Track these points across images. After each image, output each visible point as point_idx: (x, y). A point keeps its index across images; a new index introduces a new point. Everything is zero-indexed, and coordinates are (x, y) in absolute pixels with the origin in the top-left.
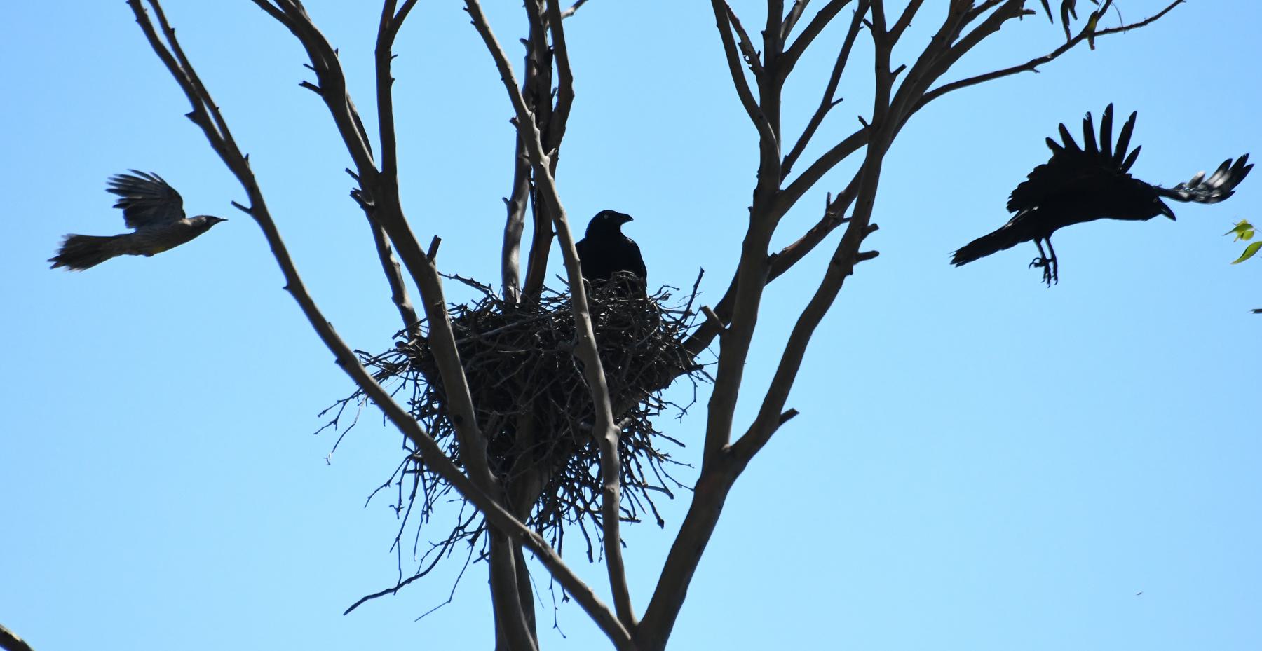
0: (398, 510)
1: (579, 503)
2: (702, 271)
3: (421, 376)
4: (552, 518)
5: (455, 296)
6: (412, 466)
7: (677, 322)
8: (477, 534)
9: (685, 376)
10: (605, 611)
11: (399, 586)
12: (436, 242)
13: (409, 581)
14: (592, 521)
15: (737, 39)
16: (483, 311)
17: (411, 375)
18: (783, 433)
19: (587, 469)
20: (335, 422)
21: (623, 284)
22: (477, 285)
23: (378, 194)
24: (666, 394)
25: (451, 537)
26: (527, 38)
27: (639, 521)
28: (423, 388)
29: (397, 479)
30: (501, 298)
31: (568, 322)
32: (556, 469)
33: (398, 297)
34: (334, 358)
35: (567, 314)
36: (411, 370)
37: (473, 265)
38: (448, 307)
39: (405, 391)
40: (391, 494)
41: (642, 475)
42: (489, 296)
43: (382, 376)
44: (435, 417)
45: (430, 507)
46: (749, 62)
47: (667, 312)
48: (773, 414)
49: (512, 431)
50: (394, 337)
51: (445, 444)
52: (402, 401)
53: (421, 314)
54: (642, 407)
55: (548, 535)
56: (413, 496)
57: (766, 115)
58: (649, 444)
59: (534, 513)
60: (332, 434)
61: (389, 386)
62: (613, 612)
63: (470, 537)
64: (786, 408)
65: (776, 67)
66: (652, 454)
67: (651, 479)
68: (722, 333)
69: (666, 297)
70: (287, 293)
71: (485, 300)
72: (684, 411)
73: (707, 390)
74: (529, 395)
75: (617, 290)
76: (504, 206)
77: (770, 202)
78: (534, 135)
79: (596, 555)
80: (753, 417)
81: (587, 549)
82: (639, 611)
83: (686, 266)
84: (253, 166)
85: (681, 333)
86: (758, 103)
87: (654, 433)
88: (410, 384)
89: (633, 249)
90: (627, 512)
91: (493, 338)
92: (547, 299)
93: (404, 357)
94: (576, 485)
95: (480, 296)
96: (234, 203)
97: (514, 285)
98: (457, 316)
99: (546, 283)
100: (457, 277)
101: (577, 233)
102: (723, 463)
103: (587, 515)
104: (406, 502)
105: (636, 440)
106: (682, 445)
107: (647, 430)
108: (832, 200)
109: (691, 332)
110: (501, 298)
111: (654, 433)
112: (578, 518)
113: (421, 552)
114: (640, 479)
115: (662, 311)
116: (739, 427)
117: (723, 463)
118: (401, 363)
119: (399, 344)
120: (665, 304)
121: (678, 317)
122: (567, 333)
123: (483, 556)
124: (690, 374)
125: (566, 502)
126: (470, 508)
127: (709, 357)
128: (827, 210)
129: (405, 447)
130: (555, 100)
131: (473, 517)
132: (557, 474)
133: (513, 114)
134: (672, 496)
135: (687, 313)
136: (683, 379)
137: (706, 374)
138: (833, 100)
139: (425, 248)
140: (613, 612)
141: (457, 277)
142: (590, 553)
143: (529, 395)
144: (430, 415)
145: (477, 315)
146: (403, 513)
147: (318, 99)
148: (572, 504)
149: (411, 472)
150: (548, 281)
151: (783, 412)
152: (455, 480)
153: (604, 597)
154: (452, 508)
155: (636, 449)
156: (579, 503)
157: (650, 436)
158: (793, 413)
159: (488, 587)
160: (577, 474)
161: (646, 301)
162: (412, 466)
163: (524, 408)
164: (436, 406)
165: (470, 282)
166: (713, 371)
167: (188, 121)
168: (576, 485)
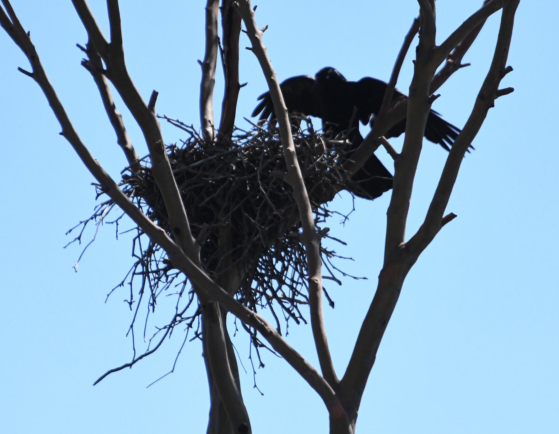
0: (131, 304)
1: (269, 292)
3: (142, 201)
5: (172, 137)
6: (140, 268)
10: (314, 372)
11: (134, 362)
13: (141, 358)
14: (280, 306)
16: (190, 145)
20: (79, 238)
23: (105, 58)
24: (331, 206)
26: (202, 61)
29: (128, 280)
33: (122, 141)
37: (182, 116)
45: (154, 301)
49: (214, 238)
56: (142, 292)
60: (77, 248)
62: (320, 373)
63: (189, 321)
64: (446, 213)
70: (62, 137)
71: (190, 139)
80: (421, 221)
82: (340, 372)
84: (33, 39)
91: (198, 167)
92: (238, 136)
94: (266, 278)
96: (20, 69)
102: (400, 257)
103: (274, 301)
104: (136, 297)
113: (149, 335)
116: (411, 229)
117: (400, 257)
123: (197, 335)
125: (259, 292)
129: (133, 255)
134: (340, 283)
139: (146, 101)
140: (320, 373)
143: (227, 210)
145: (184, 152)
146: (134, 306)
148: (263, 293)
151: (444, 215)
153: (313, 361)
156: (269, 292)
158: (452, 216)
159: (201, 361)
162: (140, 268)
163: (225, 221)
168: (266, 278)
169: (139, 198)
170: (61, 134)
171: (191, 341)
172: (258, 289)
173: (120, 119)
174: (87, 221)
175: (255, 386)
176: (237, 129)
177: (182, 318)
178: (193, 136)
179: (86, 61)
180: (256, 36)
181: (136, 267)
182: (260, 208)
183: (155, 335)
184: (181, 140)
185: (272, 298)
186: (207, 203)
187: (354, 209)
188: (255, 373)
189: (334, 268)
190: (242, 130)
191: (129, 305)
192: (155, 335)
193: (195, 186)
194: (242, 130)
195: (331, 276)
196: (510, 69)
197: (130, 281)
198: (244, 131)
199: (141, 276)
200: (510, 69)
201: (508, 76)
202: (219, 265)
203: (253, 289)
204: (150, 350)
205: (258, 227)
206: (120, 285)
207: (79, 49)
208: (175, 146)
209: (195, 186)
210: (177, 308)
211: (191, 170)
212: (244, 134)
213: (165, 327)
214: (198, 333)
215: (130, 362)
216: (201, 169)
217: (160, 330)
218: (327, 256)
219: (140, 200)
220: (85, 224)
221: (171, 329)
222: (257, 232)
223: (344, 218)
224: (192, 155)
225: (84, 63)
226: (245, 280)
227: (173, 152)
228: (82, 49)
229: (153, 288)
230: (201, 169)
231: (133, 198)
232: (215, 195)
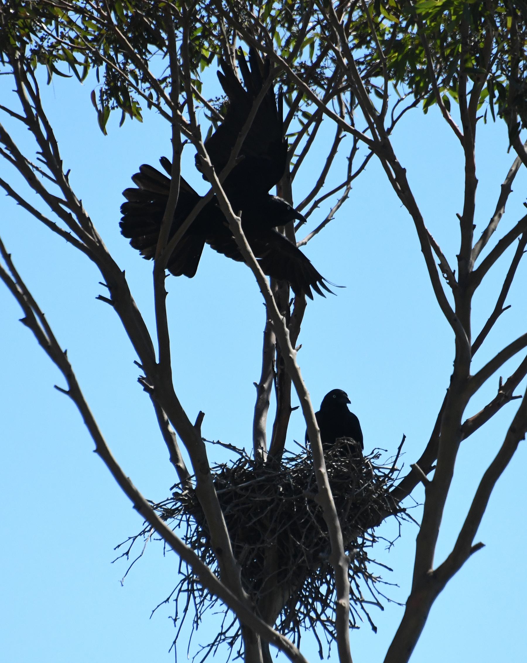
0: (175, 620)
1: (312, 614)
2: (404, 437)
3: (192, 518)
5: (218, 457)
7: (386, 476)
8: (234, 638)
9: (392, 517)
12: (201, 416)
14: (322, 628)
15: (437, 261)
16: (239, 467)
17: (184, 518)
18: (473, 562)
19: (317, 588)
20: (127, 553)
21: (344, 446)
22: (234, 449)
24: (378, 531)
25: (215, 641)
27: (358, 628)
28: (194, 527)
29: (174, 596)
30: (252, 458)
31: (307, 474)
32: (295, 588)
33: (174, 458)
34: (132, 504)
35: (301, 471)
36: (184, 513)
37: (230, 432)
38: (211, 466)
39: (182, 528)
40: (170, 609)
41: (360, 592)
42: (243, 457)
43: (165, 518)
44: (203, 549)
46: (446, 279)
47: (378, 468)
48: (465, 547)
49: (261, 559)
50: (171, 489)
52: (180, 534)
53: (191, 471)
54: (360, 541)
55: (289, 638)
57: (459, 319)
58: (365, 568)
59: (278, 622)
60: (125, 563)
61: (170, 524)
64: (474, 543)
65: (467, 282)
67: (367, 596)
68: (426, 483)
69: (377, 457)
71: (240, 460)
72: (392, 544)
73: (412, 531)
74: (273, 531)
75: (340, 452)
76: (255, 389)
77: (462, 385)
78: (285, 334)
79: (325, 654)
81: (318, 649)
83: (394, 432)
84: (71, 359)
85: (389, 484)
86: (454, 311)
87: (369, 560)
88: (184, 524)
89: (354, 421)
91: (246, 488)
92: (287, 459)
94: (310, 601)
96: (56, 387)
97: (262, 448)
98: (219, 472)
99: (287, 446)
100: (218, 442)
101: (315, 407)
102: (428, 583)
103: (318, 623)
104: (181, 615)
105: (355, 566)
106: (390, 570)
107: (364, 558)
108: (504, 383)
109: (397, 483)
110: (252, 458)
111: (369, 560)
112: (312, 625)
113: (193, 652)
114: (358, 595)
115: (374, 468)
117: (428, 583)
119: (176, 494)
120: (377, 462)
121: (387, 472)
122: (302, 484)
123: (239, 655)
124: (396, 515)
127: (416, 500)
128: (499, 390)
129: (180, 572)
130: (292, 308)
131: (232, 625)
132: (295, 592)
134: (382, 609)
135: (393, 470)
136: (391, 519)
137: (408, 515)
138: (504, 307)
141: (218, 442)
142: (321, 652)
143: (273, 531)
144: (199, 548)
146: (178, 622)
147: (110, 309)
148: (307, 615)
149: (184, 591)
150: (289, 445)
154: (219, 616)
155: (355, 573)
156: (312, 614)
157: (366, 563)
158: (480, 546)
160: (310, 592)
161: (362, 459)
162: (185, 586)
163: (270, 542)
164: (203, 541)
165: (229, 446)
166: (418, 514)
167: (21, 324)
168: (310, 601)
170: (95, 451)
174: (136, 537)
180: (291, 355)
181: (182, 584)
182: (305, 530)
183: (198, 653)
184: (231, 461)
186: (254, 523)
187: (400, 536)
190: (291, 453)
191: (173, 622)
192: (198, 653)
194: (291, 453)
195: (363, 604)
197: (175, 598)
198: (294, 454)
202: (263, 586)
203: (296, 610)
206: (165, 602)
208: (225, 465)
210: (222, 626)
212: (294, 456)
213: (209, 645)
214: (241, 653)
216: (250, 491)
217: (204, 648)
219: (189, 517)
220: (134, 540)
221: (214, 648)
222: (302, 555)
223: (389, 544)
227: (223, 471)
229: (198, 606)
230: (250, 491)
231: (182, 515)
232: (263, 515)
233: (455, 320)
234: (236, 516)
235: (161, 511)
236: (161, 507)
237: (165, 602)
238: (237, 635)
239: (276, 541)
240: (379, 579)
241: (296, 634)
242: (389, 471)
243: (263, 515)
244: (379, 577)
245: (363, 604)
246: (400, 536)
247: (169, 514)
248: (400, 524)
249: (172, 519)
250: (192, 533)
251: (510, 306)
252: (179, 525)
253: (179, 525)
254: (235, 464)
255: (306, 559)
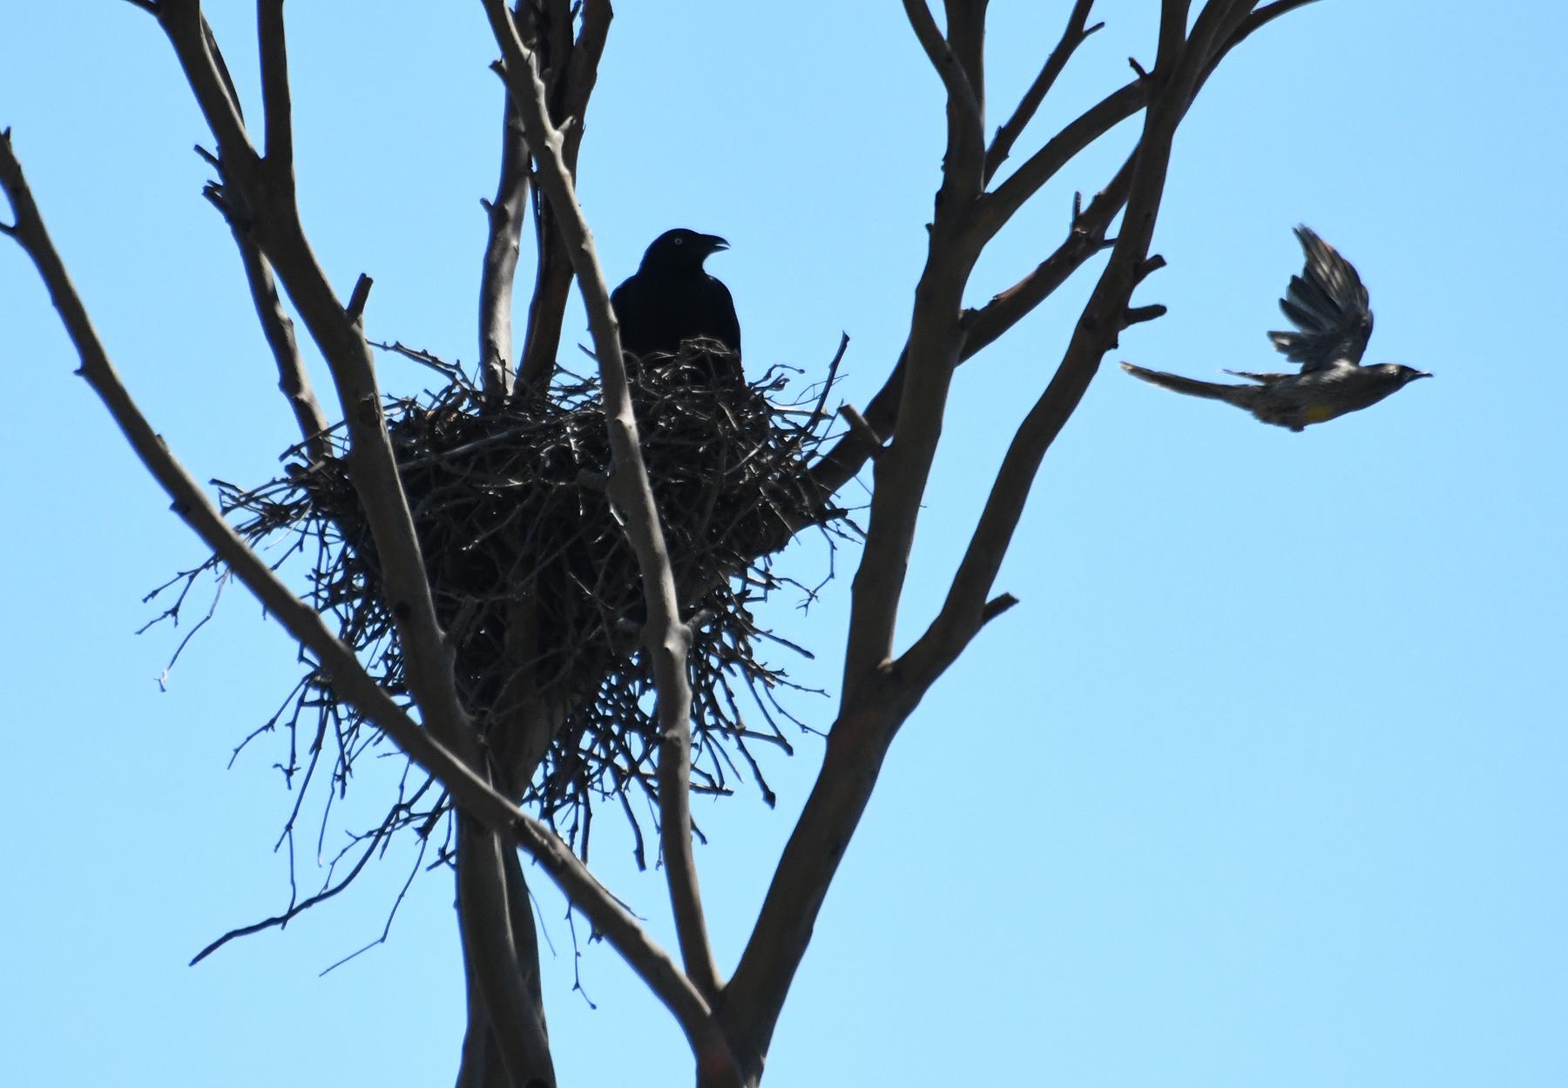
0: (289, 773)
1: (620, 761)
2: (846, 339)
3: (332, 528)
4: (570, 789)
5: (400, 383)
13: (309, 903)
20: (174, 612)
24: (780, 563)
26: (492, 201)
27: (729, 793)
32: (578, 699)
33: (290, 382)
36: (313, 516)
39: (300, 557)
45: (347, 768)
48: (971, 604)
51: (373, 657)
52: (296, 582)
56: (317, 746)
59: (538, 778)
61: (269, 549)
63: (420, 823)
64: (994, 593)
66: (754, 672)
67: (752, 719)
69: (778, 385)
71: (448, 390)
78: (534, 93)
83: (815, 327)
85: (806, 449)
88: (312, 543)
90: (709, 777)
91: (464, 459)
93: (301, 493)
94: (615, 729)
95: (440, 382)
99: (560, 359)
102: (880, 693)
104: (304, 759)
107: (743, 627)
109: (825, 448)
112: (618, 788)
113: (331, 851)
115: (772, 411)
117: (880, 693)
118: (296, 505)
120: (777, 399)
121: (803, 421)
123: (444, 857)
124: (823, 525)
125: (597, 758)
126: (418, 775)
127: (856, 494)
128: (1075, 224)
129: (302, 658)
130: (578, 24)
133: (496, 54)
134: (790, 750)
137: (851, 524)
142: (640, 853)
146: (297, 779)
148: (607, 762)
152: (393, 724)
154: (385, 771)
156: (620, 761)
158: (1006, 602)
159: (453, 915)
163: (521, 589)
166: (863, 519)
168: (615, 729)
169: (322, 522)
170: (78, 372)
171: (430, 868)
172: (596, 751)
173: (288, 331)
174: (197, 572)
175: (577, 986)
176: (560, 370)
177: (412, 815)
178: (456, 383)
179: (216, 186)
180: (548, 144)
184: (427, 391)
185: (628, 776)
187: (832, 576)
188: (578, 954)
189: (780, 711)
191: (284, 776)
193: (459, 501)
196: (1159, 262)
199: (316, 710)
200: (1159, 262)
201: (1153, 278)
202: (502, 694)
203: (583, 751)
204: (331, 888)
205: (599, 606)
206: (266, 728)
207: (200, 158)
208: (414, 402)
209: (459, 501)
210: (402, 787)
211: (445, 465)
212: (580, 383)
213: (370, 834)
214: (448, 851)
215: (282, 912)
218: (767, 684)
219: (325, 526)
221: (383, 839)
222: (598, 620)
224: (453, 426)
225: (210, 192)
226: (566, 726)
228: (208, 157)
229: (345, 738)
231: (308, 520)
232: (504, 525)
233: (950, 60)
234: (438, 525)
235: (256, 510)
236: (257, 500)
237: (266, 728)
238: (438, 810)
239: (533, 586)
240: (780, 677)
241: (582, 808)
242: (808, 419)
243: (504, 525)
244: (781, 672)
245: (744, 739)
246: (832, 576)
247: (275, 516)
248: (833, 547)
249: (285, 530)
250: (332, 563)
251: (1101, 25)
252: (300, 544)
253: (300, 544)
254: (436, 399)
255: (606, 630)
